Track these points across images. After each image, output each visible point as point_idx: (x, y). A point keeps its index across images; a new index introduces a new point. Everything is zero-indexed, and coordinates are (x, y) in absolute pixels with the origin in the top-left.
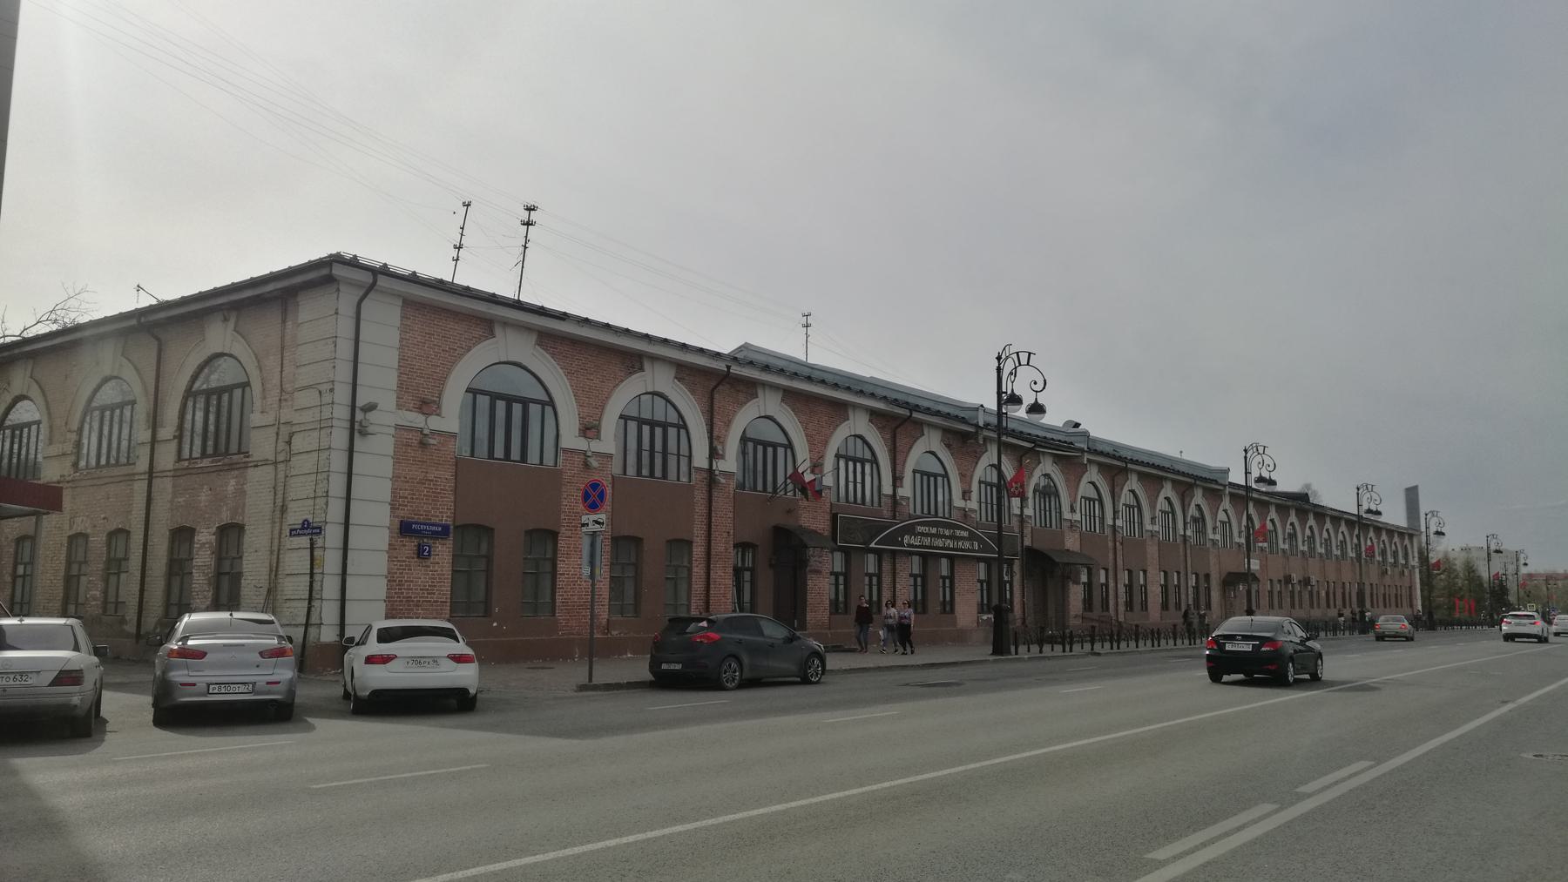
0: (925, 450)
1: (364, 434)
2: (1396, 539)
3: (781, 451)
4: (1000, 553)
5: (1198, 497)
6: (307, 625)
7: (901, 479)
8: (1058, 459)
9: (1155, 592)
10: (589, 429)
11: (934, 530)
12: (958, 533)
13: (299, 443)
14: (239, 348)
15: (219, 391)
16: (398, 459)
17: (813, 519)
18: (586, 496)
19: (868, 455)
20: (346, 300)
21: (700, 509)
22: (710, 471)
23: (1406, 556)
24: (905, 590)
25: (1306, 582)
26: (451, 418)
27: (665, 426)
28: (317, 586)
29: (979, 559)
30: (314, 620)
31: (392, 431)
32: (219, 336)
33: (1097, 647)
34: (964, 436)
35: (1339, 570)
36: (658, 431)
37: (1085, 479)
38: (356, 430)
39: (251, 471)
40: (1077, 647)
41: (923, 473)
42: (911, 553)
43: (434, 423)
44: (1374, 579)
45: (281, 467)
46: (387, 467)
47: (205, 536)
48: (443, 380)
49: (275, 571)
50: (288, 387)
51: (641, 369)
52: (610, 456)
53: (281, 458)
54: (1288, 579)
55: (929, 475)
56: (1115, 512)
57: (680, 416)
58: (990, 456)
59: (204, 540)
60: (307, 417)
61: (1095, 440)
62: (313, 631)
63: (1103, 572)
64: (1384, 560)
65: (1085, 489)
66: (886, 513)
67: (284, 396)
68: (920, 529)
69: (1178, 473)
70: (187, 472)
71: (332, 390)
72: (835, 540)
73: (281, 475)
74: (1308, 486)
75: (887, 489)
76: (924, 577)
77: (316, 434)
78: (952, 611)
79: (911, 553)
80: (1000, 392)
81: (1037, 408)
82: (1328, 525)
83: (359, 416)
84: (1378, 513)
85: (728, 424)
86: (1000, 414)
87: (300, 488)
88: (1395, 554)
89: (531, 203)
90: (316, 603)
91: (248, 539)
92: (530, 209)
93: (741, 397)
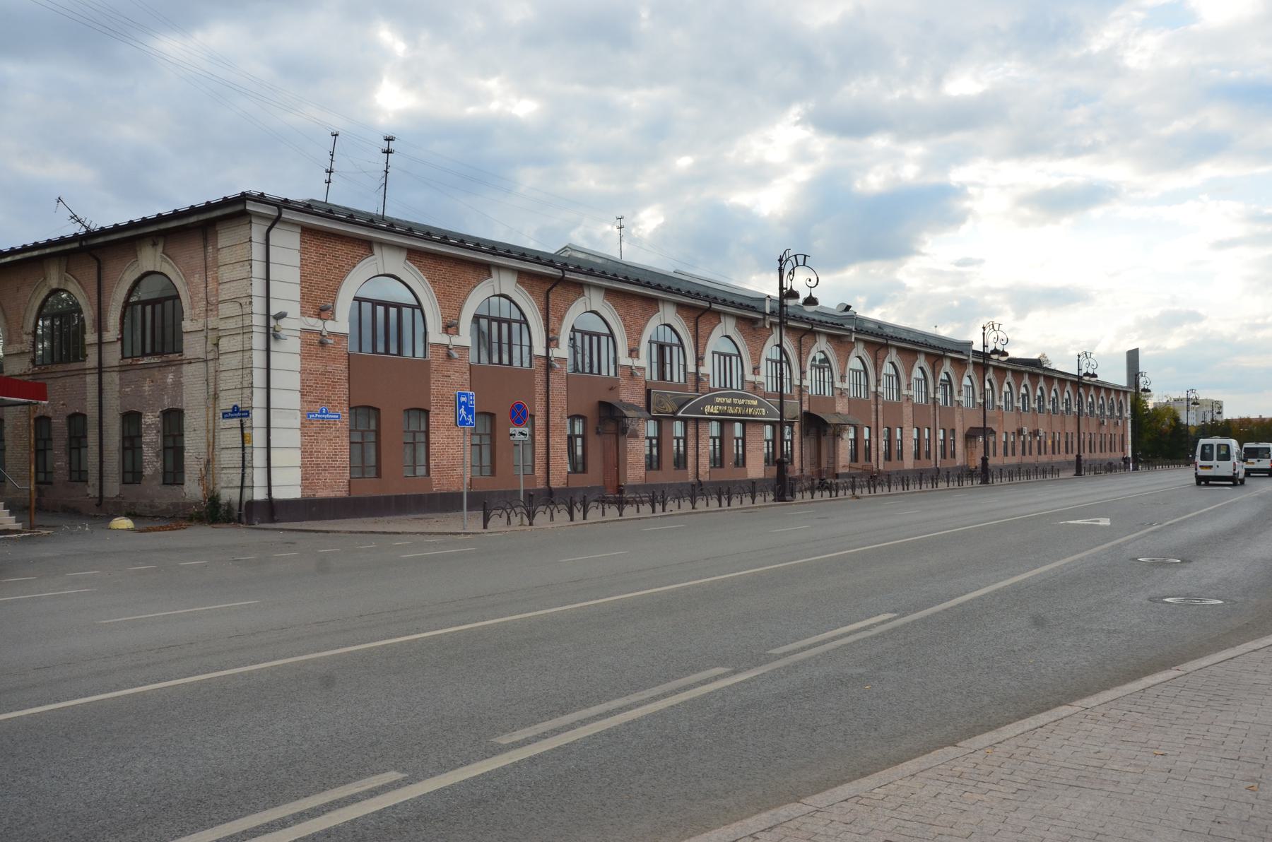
0: (723, 335)
1: (277, 337)
2: (1113, 395)
3: (604, 339)
4: (782, 416)
5: (947, 366)
6: (242, 487)
7: (702, 359)
8: (831, 337)
9: (910, 446)
10: (450, 327)
11: (729, 401)
12: (749, 402)
13: (225, 344)
14: (167, 269)
15: (153, 302)
16: (305, 356)
17: (630, 395)
18: (512, 414)
19: (675, 340)
20: (257, 231)
21: (540, 389)
22: (547, 357)
23: (1120, 410)
24: (707, 447)
25: (1035, 433)
26: (342, 322)
27: (509, 322)
28: (248, 457)
29: (766, 423)
30: (247, 483)
31: (298, 334)
32: (150, 259)
33: (858, 492)
34: (753, 321)
35: (1063, 423)
36: (505, 326)
37: (853, 354)
38: (271, 335)
39: (186, 368)
40: (841, 493)
41: (720, 354)
42: (711, 420)
43: (330, 326)
44: (1093, 430)
45: (211, 364)
46: (296, 363)
47: (151, 419)
48: (335, 291)
49: (212, 445)
50: (212, 299)
51: (490, 276)
52: (467, 348)
53: (210, 356)
54: (1020, 432)
55: (725, 355)
56: (878, 381)
57: (522, 313)
58: (774, 339)
59: (150, 422)
60: (231, 324)
61: (863, 320)
62: (247, 492)
63: (866, 430)
64: (1103, 413)
65: (854, 363)
66: (691, 387)
67: (211, 307)
68: (718, 400)
69: (930, 346)
70: (132, 367)
71: (251, 303)
72: (648, 410)
73: (212, 370)
74: (1043, 355)
75: (691, 368)
76: (721, 438)
77: (239, 338)
78: (744, 464)
79: (711, 420)
80: (781, 288)
81: (811, 301)
82: (1056, 385)
83: (273, 323)
84: (1094, 376)
85: (561, 319)
86: (782, 305)
87: (228, 382)
88: (1112, 409)
89: (389, 134)
90: (248, 471)
91: (187, 421)
92: (388, 140)
93: (571, 295)
